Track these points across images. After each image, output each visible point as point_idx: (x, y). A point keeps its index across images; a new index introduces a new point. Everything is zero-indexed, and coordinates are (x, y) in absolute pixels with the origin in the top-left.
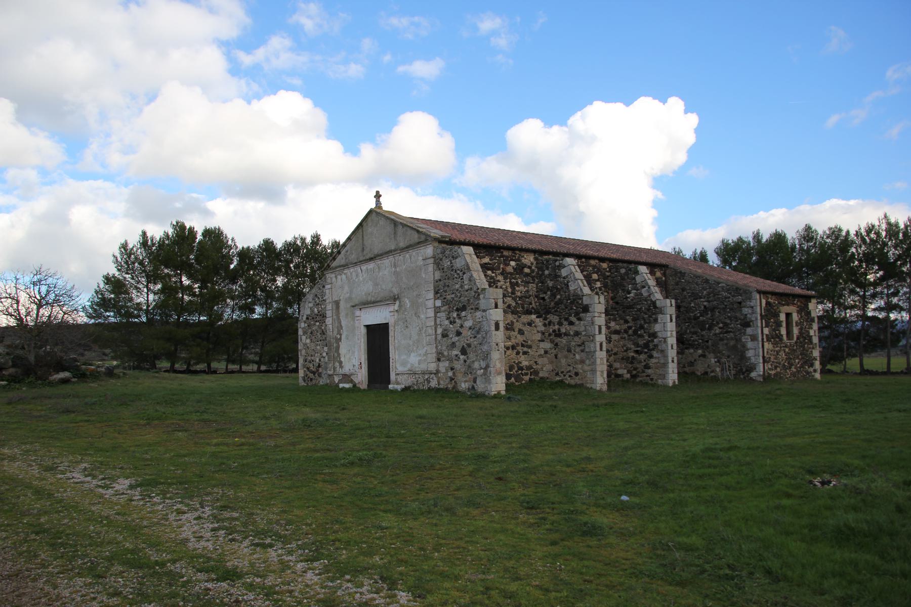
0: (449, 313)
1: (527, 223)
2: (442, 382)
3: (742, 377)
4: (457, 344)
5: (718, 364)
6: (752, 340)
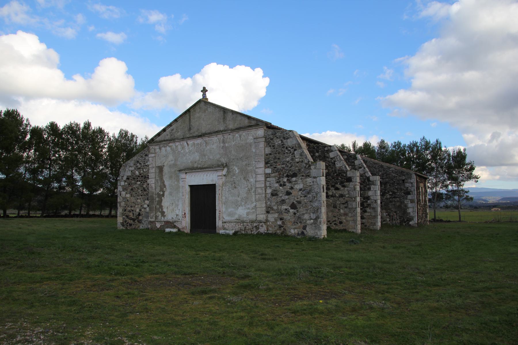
0: (279, 178)
2: (270, 229)
3: (404, 224)
4: (287, 201)
5: (388, 216)
6: (411, 203)
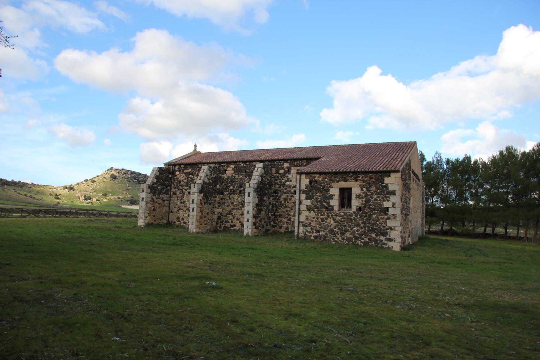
1: (215, 139)
